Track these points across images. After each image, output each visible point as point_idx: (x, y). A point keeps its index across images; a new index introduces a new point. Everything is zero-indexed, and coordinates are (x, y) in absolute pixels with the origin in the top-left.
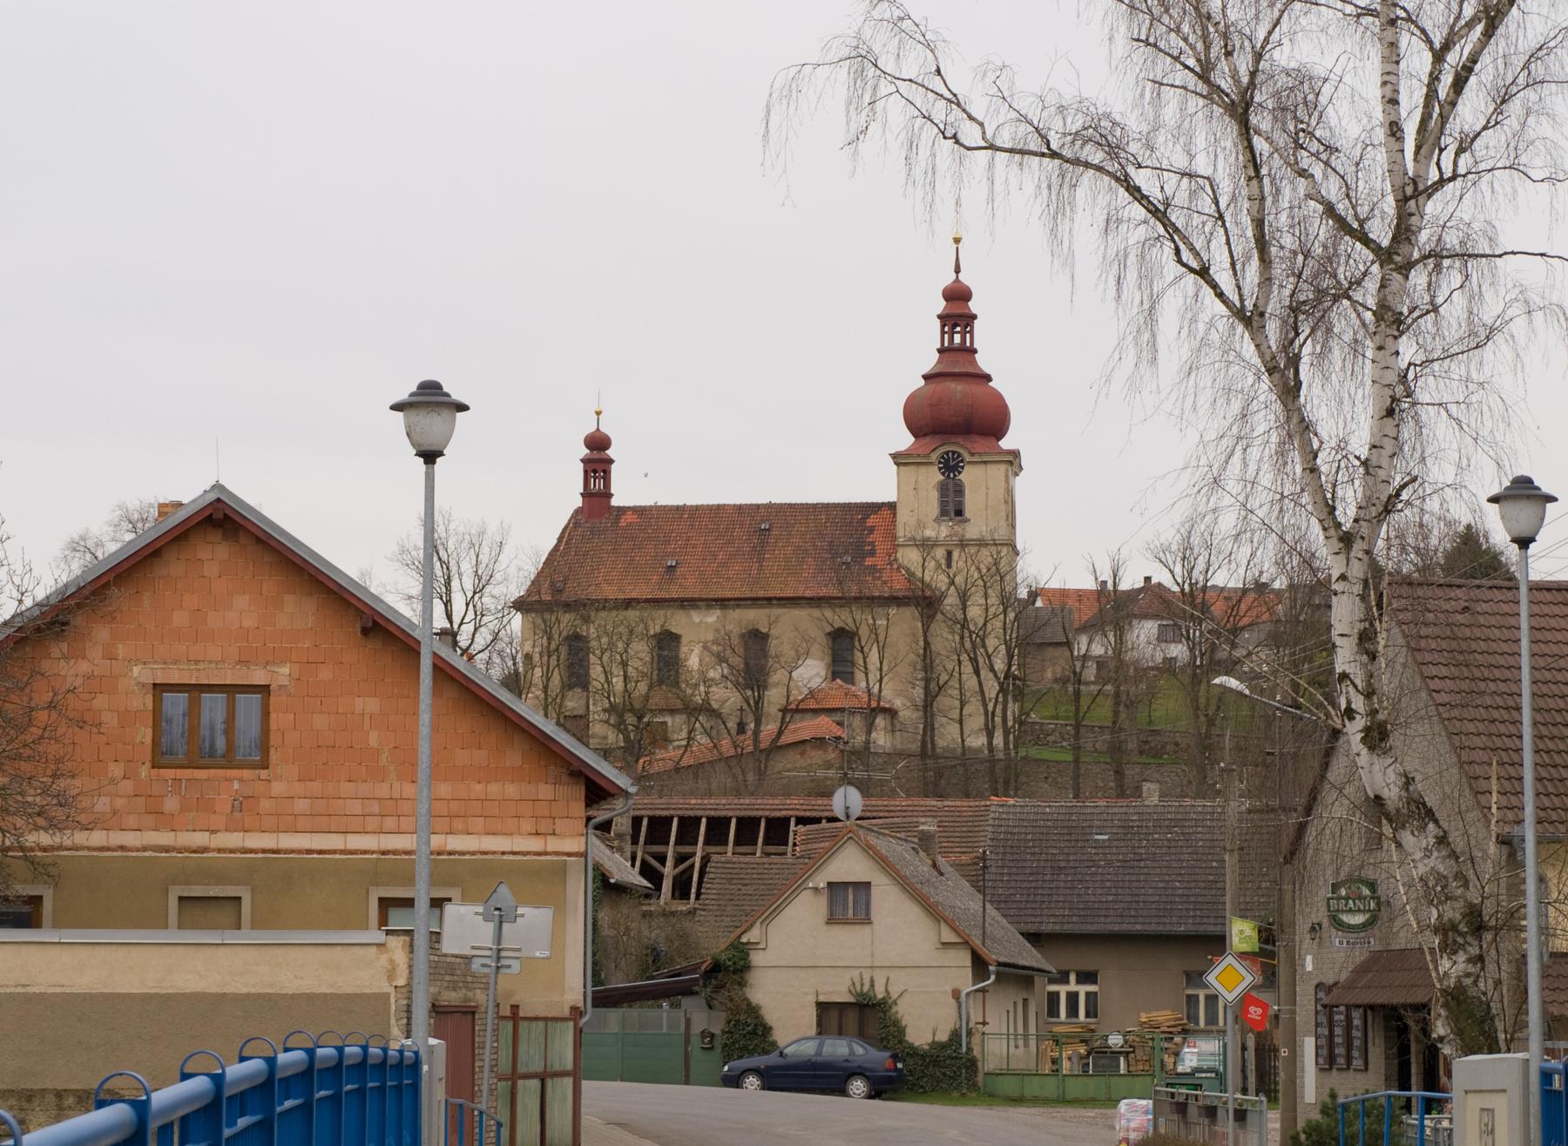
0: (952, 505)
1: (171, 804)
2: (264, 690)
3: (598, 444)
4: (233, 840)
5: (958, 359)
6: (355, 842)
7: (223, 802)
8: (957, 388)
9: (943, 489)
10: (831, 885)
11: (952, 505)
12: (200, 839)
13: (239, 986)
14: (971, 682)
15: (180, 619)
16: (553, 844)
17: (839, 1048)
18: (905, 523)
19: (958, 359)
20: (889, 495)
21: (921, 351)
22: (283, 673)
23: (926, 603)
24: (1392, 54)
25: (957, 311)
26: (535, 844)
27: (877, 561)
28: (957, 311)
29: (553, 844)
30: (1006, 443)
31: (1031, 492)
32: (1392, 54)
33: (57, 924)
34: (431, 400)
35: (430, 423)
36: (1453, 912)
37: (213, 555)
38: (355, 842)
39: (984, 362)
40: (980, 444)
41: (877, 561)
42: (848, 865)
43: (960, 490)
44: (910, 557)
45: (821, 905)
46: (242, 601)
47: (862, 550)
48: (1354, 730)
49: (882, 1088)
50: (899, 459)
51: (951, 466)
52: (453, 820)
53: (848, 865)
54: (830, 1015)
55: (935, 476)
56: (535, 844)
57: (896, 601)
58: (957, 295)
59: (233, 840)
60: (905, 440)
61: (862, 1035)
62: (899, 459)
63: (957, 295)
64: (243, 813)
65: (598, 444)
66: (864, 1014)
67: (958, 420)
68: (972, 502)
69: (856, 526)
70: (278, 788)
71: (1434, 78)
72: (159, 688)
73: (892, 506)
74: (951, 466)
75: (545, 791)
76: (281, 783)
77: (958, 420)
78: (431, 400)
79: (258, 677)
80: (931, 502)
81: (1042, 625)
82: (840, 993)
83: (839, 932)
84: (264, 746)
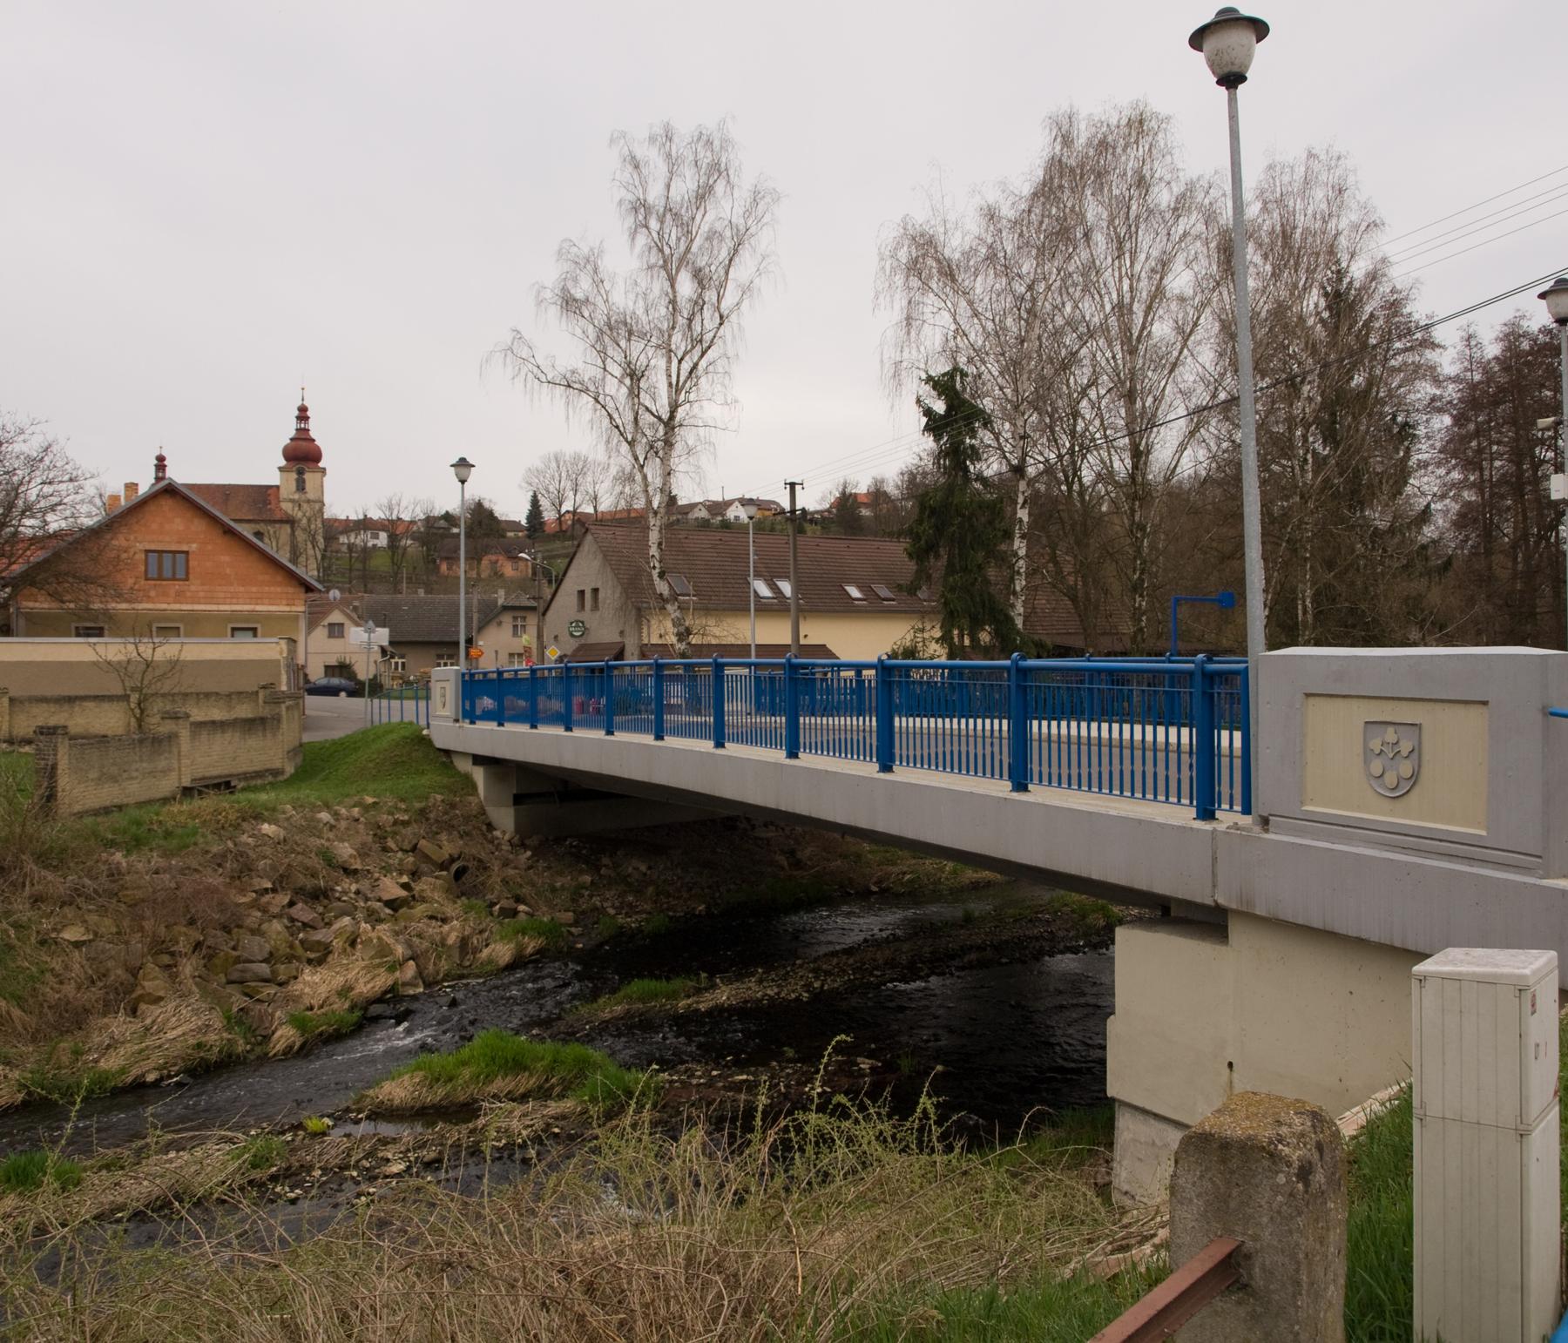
0: (301, 486)
1: (153, 593)
2: (187, 553)
3: (161, 459)
4: (177, 606)
5: (303, 435)
6: (222, 607)
7: (172, 592)
8: (303, 444)
9: (297, 481)
10: (330, 625)
11: (301, 486)
12: (164, 606)
13: (229, 657)
14: (311, 552)
15: (154, 526)
16: (294, 609)
17: (335, 681)
18: (283, 493)
19: (303, 435)
20: (277, 483)
21: (289, 429)
22: (194, 546)
23: (291, 522)
24: (669, 361)
25: (303, 413)
26: (287, 609)
27: (272, 506)
28: (303, 413)
29: (294, 609)
30: (321, 465)
31: (328, 481)
32: (669, 361)
33: (186, 635)
34: (463, 464)
35: (463, 471)
36: (682, 629)
37: (167, 504)
38: (222, 607)
39: (313, 434)
40: (311, 465)
41: (272, 506)
42: (336, 617)
43: (304, 481)
44: (284, 506)
45: (326, 631)
46: (178, 520)
47: (266, 502)
48: (655, 573)
49: (351, 694)
50: (280, 469)
51: (300, 473)
52: (258, 599)
53: (336, 617)
54: (329, 670)
55: (294, 476)
56: (287, 609)
57: (281, 521)
58: (303, 410)
59: (177, 606)
60: (283, 463)
61: (341, 676)
62: (280, 469)
63: (303, 410)
64: (180, 597)
65: (161, 459)
66: (342, 669)
67: (303, 456)
68: (308, 486)
69: (261, 496)
70: (193, 588)
71: (668, 369)
72: (147, 551)
73: (278, 487)
74: (300, 473)
75: (291, 590)
76: (194, 586)
77: (303, 456)
78: (463, 464)
79: (185, 548)
80: (293, 486)
81: (334, 529)
82: (333, 662)
83: (332, 641)
84: (187, 573)
